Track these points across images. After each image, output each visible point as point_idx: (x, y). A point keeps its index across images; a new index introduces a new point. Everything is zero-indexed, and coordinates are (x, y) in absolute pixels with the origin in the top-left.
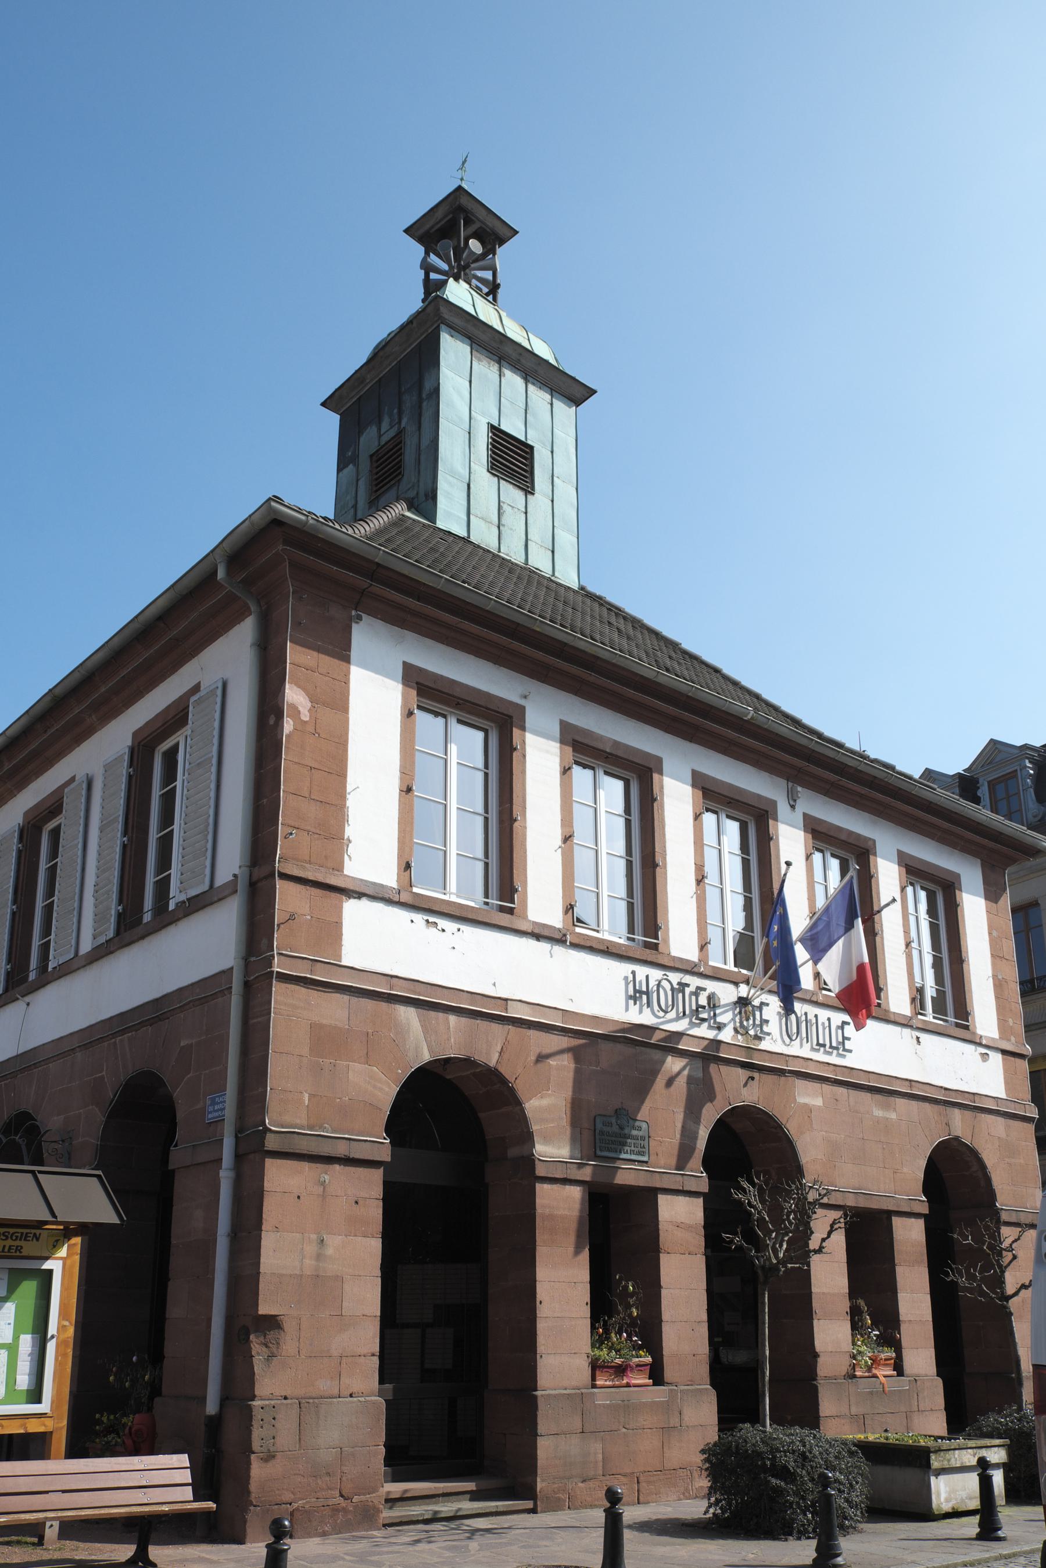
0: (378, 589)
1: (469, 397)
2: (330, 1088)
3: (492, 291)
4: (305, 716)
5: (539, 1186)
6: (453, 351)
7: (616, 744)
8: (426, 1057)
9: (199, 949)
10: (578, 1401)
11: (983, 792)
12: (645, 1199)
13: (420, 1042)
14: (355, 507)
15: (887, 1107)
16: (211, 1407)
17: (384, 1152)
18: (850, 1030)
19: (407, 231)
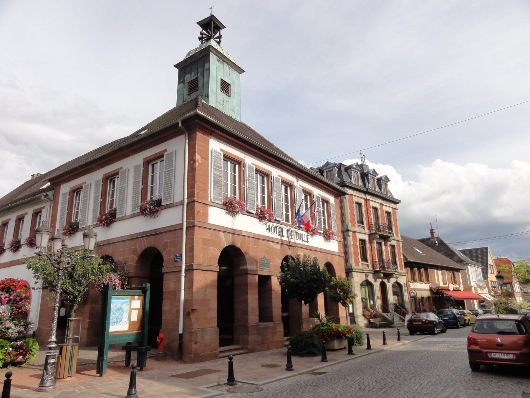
0: (217, 131)
1: (216, 71)
3: (219, 43)
4: (200, 162)
6: (213, 58)
7: (263, 168)
8: (226, 245)
10: (257, 326)
11: (325, 174)
12: (268, 278)
13: (225, 242)
14: (183, 95)
16: (181, 332)
17: (218, 268)
18: (309, 237)
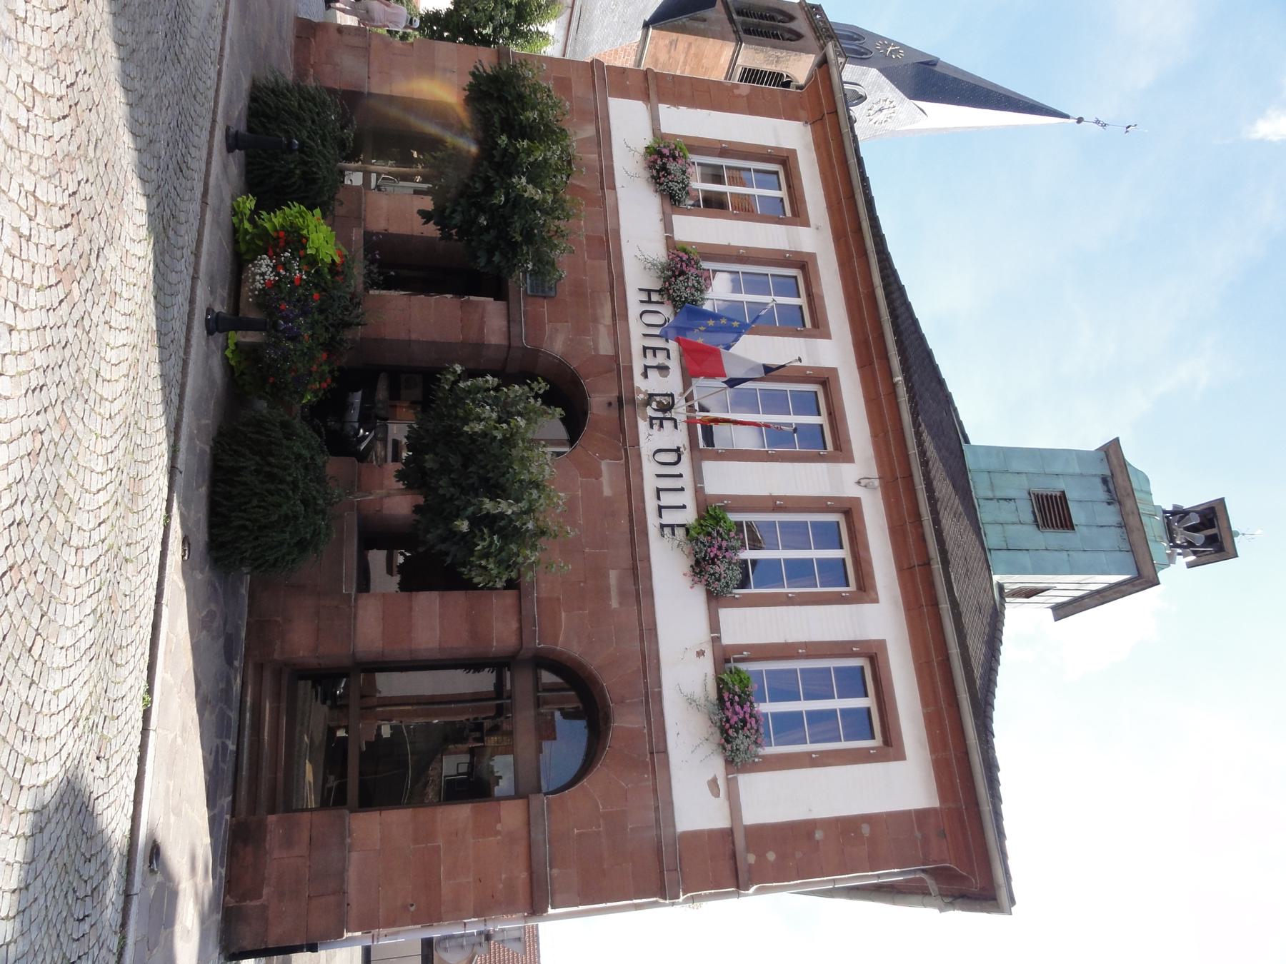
19: (1222, 501)
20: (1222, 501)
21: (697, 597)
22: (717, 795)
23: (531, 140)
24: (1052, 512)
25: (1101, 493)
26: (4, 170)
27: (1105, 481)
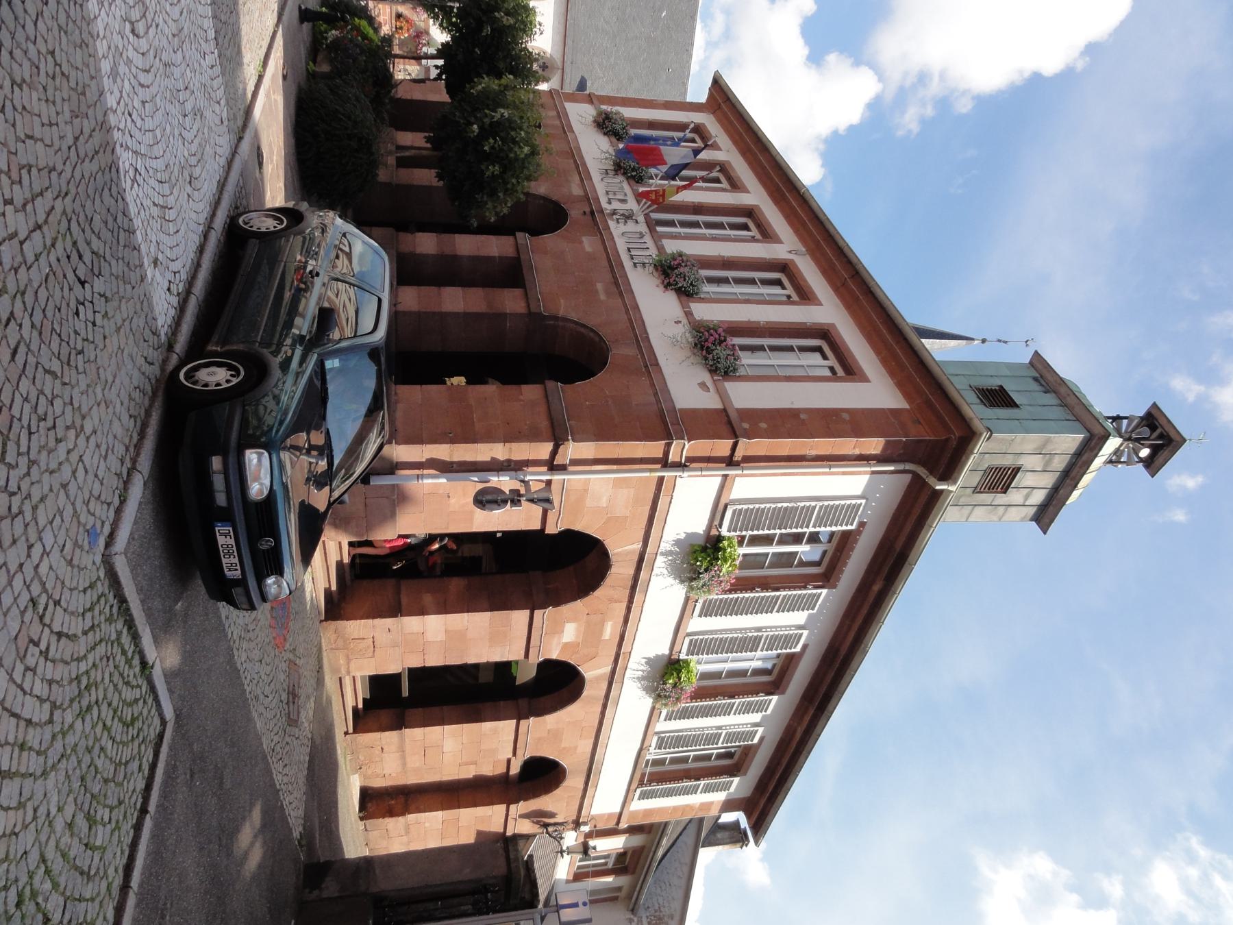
2: (591, 493)
5: (527, 612)
9: (687, 387)
15: (608, 293)
19: (1155, 405)
20: (1155, 405)
21: (671, 298)
22: (708, 390)
23: (515, 76)
24: (997, 397)
25: (1034, 386)
26: (4, 342)
27: (1036, 379)
